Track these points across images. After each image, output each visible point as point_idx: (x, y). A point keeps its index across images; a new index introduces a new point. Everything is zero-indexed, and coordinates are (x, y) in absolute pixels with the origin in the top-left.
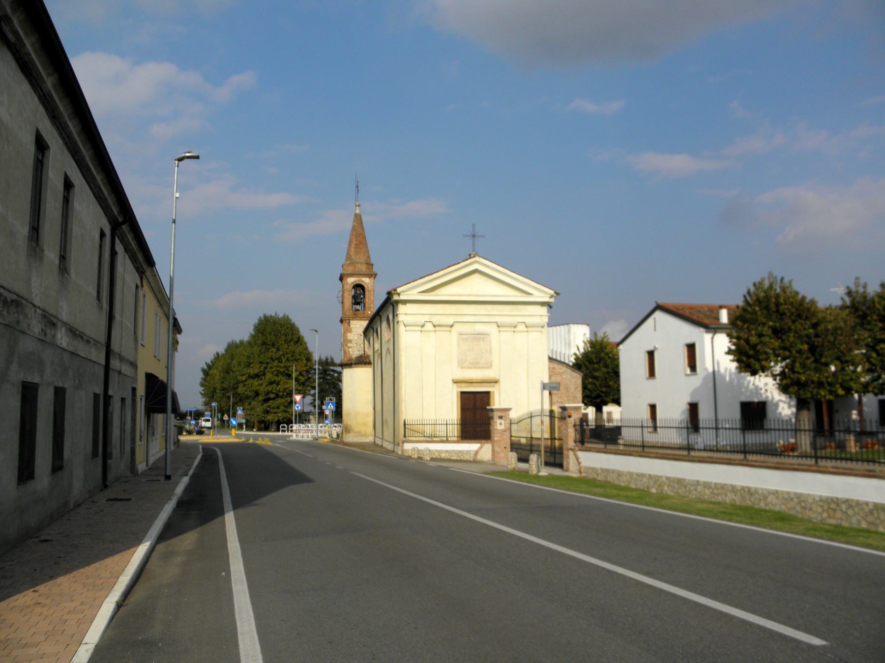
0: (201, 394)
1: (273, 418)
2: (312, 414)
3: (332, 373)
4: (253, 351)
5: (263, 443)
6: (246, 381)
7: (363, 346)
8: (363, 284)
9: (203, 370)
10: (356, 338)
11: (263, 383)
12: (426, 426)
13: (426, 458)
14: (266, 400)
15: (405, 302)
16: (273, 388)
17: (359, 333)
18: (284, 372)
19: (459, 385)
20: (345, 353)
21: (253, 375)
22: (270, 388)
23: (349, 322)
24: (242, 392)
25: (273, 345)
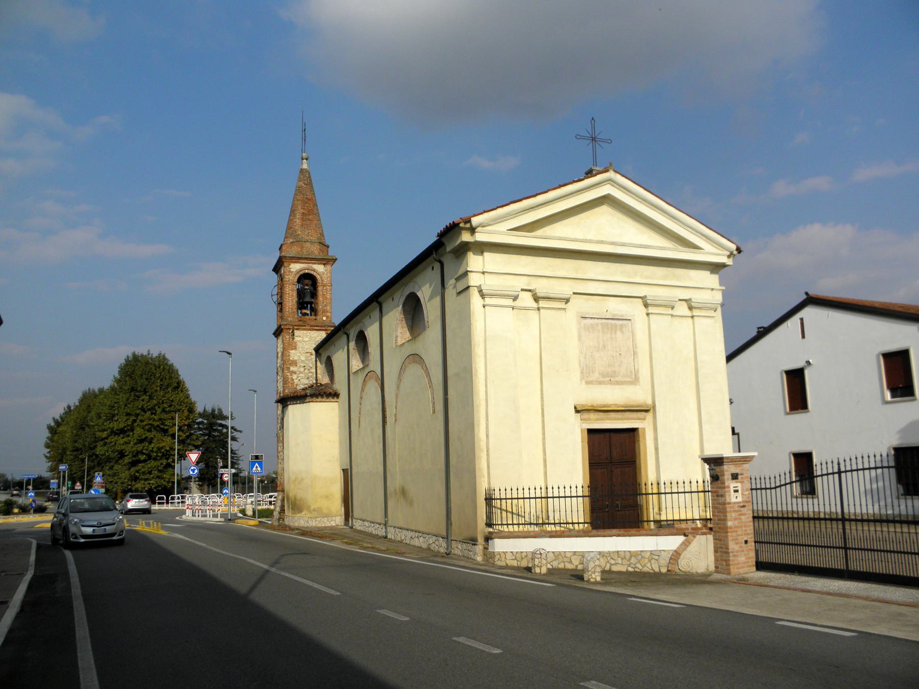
0: (46, 457)
1: (143, 486)
4: (119, 399)
5: (147, 529)
6: (106, 438)
7: (314, 370)
8: (315, 274)
9: (50, 428)
10: (303, 358)
11: (130, 441)
12: (504, 501)
13: (594, 576)
14: (134, 464)
15: (482, 248)
16: (143, 447)
17: (308, 351)
18: (158, 426)
19: (586, 415)
20: (285, 381)
21: (117, 430)
22: (140, 447)
23: (293, 332)
24: (101, 453)
25: (145, 392)
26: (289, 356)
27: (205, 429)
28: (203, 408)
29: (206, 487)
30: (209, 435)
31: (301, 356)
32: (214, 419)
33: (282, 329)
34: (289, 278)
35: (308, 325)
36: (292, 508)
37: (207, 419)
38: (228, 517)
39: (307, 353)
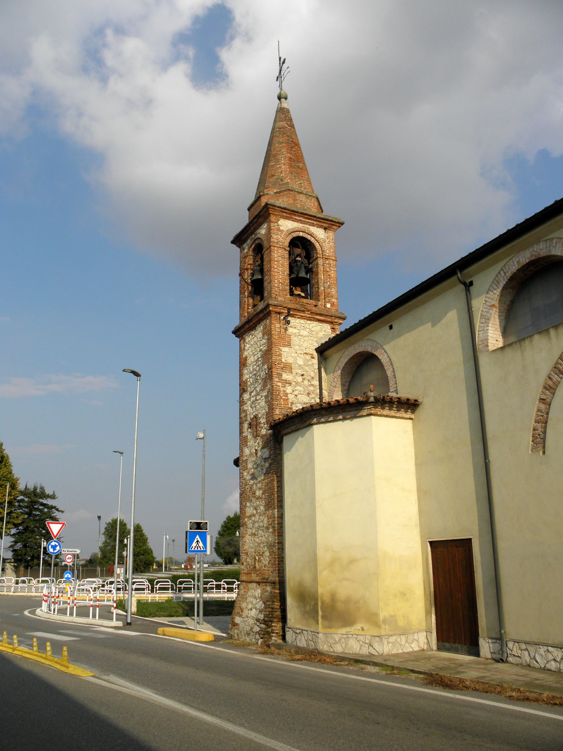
2: (9, 561)
3: (41, 507)
7: (317, 383)
8: (312, 240)
10: (301, 362)
26: (280, 355)
27: (26, 507)
28: (25, 486)
29: (22, 568)
30: (30, 514)
31: (298, 358)
32: (36, 497)
33: (269, 313)
34: (277, 239)
35: (308, 311)
36: (323, 617)
37: (28, 497)
38: (99, 609)
39: (306, 353)
